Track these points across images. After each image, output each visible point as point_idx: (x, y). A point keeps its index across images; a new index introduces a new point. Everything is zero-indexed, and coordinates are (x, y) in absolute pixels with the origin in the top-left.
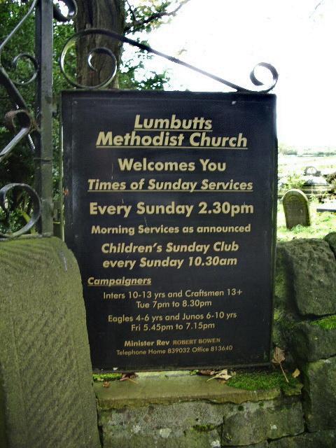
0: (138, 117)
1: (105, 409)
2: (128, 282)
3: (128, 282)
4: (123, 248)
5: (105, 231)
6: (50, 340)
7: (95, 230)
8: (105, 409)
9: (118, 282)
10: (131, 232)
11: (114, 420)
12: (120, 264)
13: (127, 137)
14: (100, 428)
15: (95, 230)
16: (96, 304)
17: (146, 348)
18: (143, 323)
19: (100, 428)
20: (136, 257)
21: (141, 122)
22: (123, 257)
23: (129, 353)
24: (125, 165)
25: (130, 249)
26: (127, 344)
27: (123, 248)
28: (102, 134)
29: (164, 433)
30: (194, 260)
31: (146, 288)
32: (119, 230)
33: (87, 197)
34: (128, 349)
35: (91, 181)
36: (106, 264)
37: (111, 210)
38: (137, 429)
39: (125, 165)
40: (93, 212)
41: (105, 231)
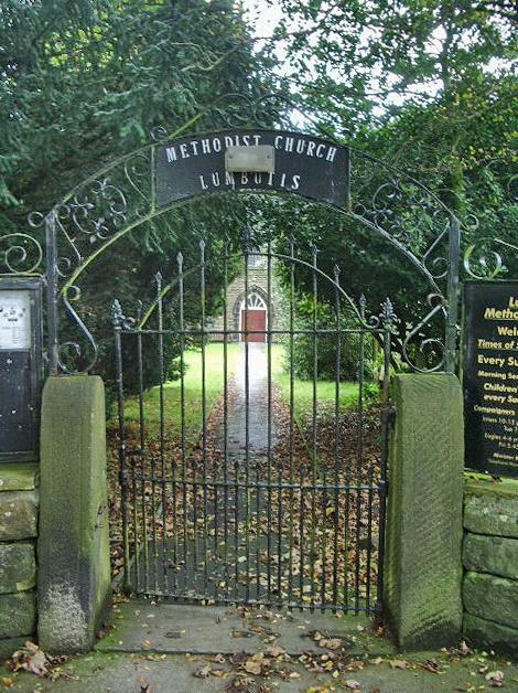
0: (512, 299)
1: (469, 493)
2: (499, 412)
3: (499, 412)
4: (497, 387)
5: (487, 375)
6: (436, 437)
7: (481, 373)
8: (469, 493)
9: (493, 410)
10: (504, 377)
11: (473, 502)
12: (495, 398)
13: (504, 311)
14: (464, 505)
15: (481, 373)
16: (474, 424)
17: (508, 460)
18: (507, 442)
19: (464, 505)
20: (505, 394)
21: (514, 302)
22: (497, 393)
23: (496, 462)
24: (502, 331)
25: (503, 388)
26: (496, 455)
27: (497, 387)
28: (488, 310)
29: (504, 518)
30: (211, 144)
31: (512, 417)
32: (496, 375)
33: (478, 351)
34: (496, 459)
35: (480, 341)
36: (486, 397)
37: (492, 361)
38: (486, 511)
39: (502, 331)
40: (480, 361)
41: (487, 375)
